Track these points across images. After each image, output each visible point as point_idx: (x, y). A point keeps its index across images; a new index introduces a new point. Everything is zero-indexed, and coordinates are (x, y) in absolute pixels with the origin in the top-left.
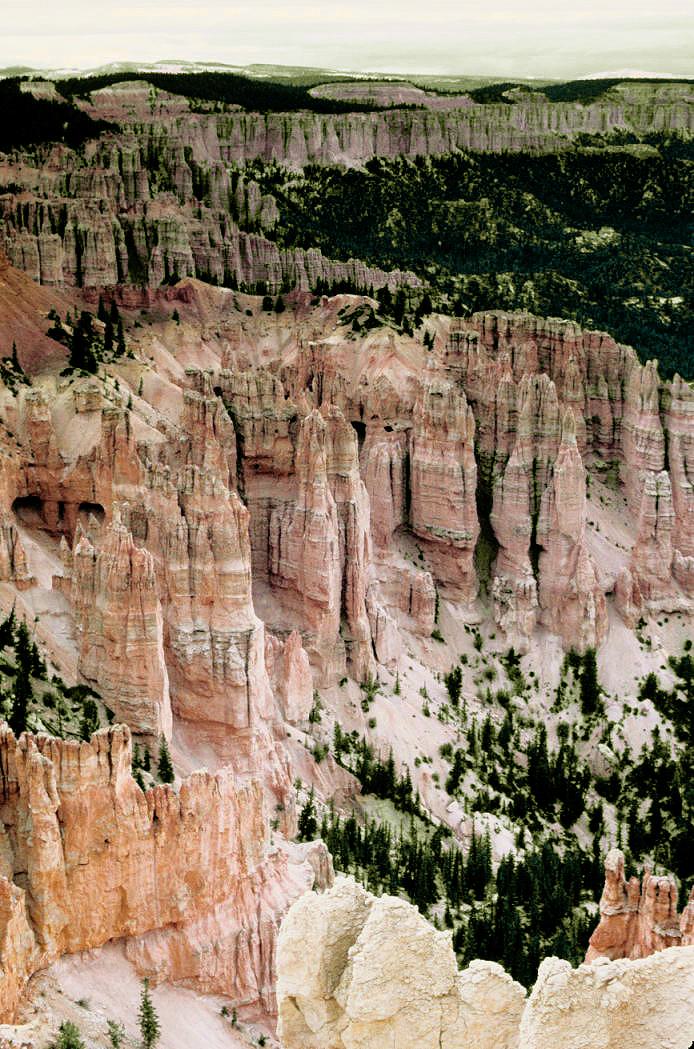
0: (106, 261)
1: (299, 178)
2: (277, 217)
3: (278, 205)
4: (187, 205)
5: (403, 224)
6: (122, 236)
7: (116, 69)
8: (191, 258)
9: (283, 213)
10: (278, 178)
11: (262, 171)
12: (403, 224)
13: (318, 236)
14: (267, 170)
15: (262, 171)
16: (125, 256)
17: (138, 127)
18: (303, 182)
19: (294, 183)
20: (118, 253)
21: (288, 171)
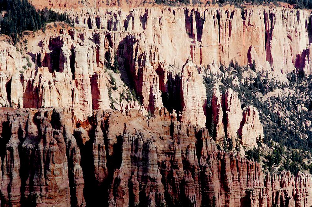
0: (56, 187)
1: (283, 87)
2: (260, 132)
3: (261, 117)
4: (158, 116)
5: (207, 185)
6: (78, 156)
7: (200, 58)
8: (160, 183)
9: (266, 129)
10: (260, 85)
11: (240, 78)
12: (207, 185)
13: (307, 157)
14: (246, 74)
15: (240, 78)
16: (81, 180)
17: (93, 20)
18: (289, 92)
19: (277, 92)
20: (72, 176)
21: (270, 77)
